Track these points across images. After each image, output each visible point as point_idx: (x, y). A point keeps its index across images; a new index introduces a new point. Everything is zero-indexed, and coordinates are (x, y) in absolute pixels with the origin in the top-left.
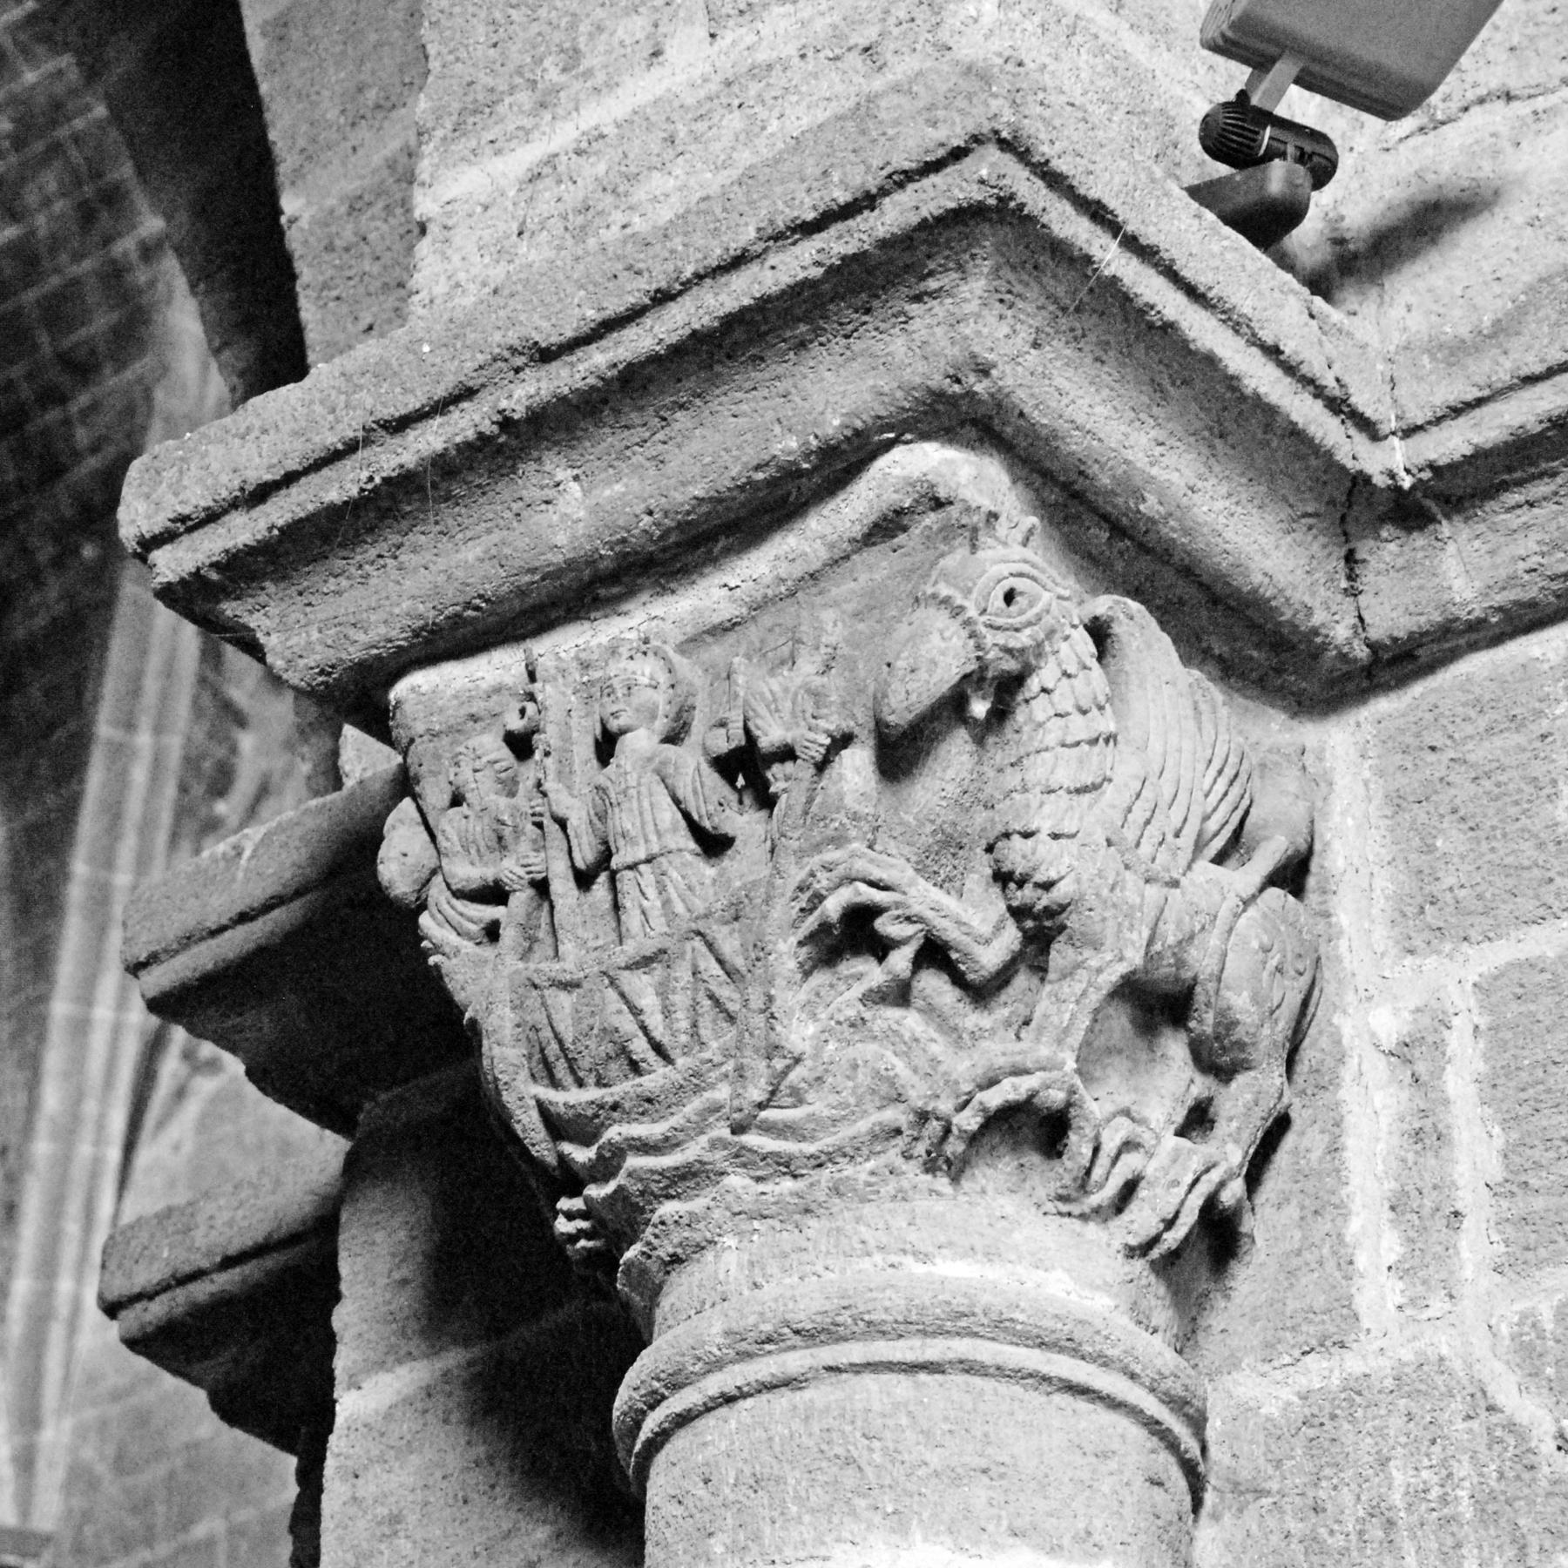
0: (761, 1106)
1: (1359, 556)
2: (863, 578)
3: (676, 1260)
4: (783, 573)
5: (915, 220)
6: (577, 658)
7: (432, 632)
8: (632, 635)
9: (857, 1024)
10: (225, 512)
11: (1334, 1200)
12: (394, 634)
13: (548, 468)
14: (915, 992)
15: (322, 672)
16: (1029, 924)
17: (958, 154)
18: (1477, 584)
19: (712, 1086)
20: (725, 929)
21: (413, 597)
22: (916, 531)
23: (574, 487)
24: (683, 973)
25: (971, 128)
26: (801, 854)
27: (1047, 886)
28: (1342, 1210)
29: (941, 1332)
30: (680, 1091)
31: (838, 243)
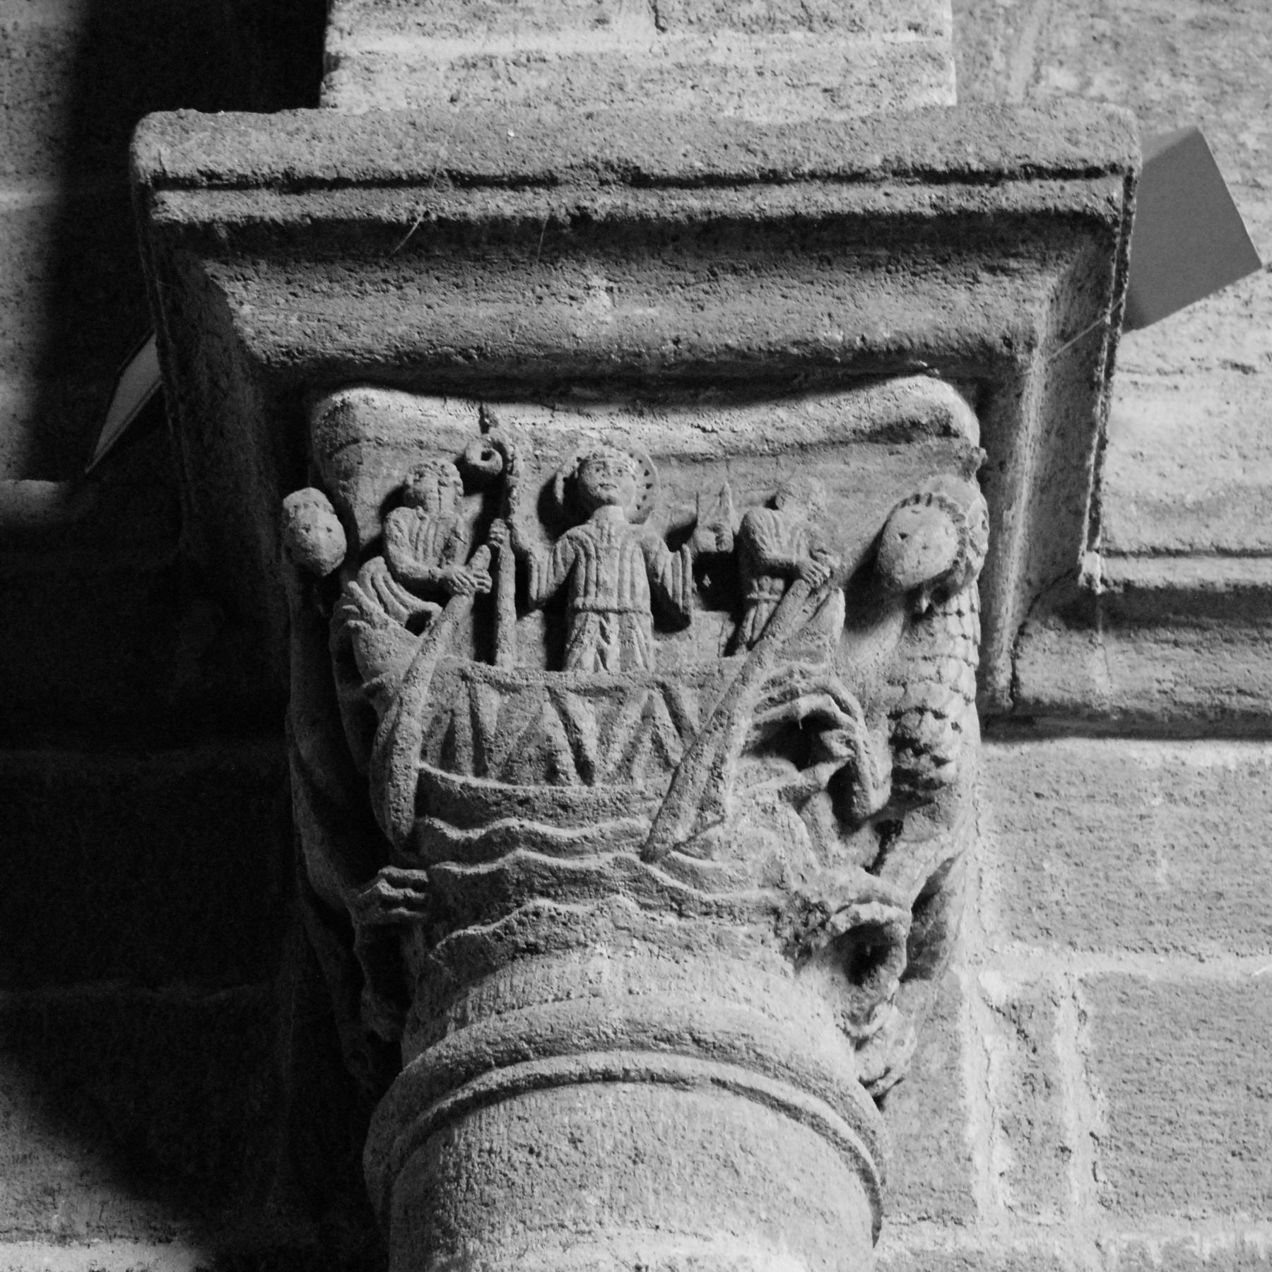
0: (677, 847)
1: (1027, 630)
2: (854, 464)
3: (533, 949)
4: (769, 435)
5: (1038, 205)
6: (532, 434)
7: (413, 361)
8: (595, 435)
9: (769, 811)
10: (257, 186)
11: (951, 1106)
12: (377, 347)
13: (586, 271)
14: (809, 806)
15: (288, 354)
16: (906, 787)
17: (1092, 173)
18: (1116, 686)
19: (633, 815)
20: (689, 691)
21: (411, 325)
22: (917, 446)
23: (605, 298)
24: (633, 713)
25: (1114, 158)
26: (781, 654)
27: (940, 762)
28: (961, 1118)
29: (806, 1087)
30: (598, 810)
31: (956, 197)
